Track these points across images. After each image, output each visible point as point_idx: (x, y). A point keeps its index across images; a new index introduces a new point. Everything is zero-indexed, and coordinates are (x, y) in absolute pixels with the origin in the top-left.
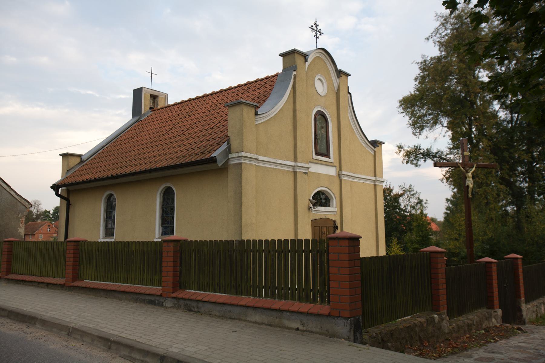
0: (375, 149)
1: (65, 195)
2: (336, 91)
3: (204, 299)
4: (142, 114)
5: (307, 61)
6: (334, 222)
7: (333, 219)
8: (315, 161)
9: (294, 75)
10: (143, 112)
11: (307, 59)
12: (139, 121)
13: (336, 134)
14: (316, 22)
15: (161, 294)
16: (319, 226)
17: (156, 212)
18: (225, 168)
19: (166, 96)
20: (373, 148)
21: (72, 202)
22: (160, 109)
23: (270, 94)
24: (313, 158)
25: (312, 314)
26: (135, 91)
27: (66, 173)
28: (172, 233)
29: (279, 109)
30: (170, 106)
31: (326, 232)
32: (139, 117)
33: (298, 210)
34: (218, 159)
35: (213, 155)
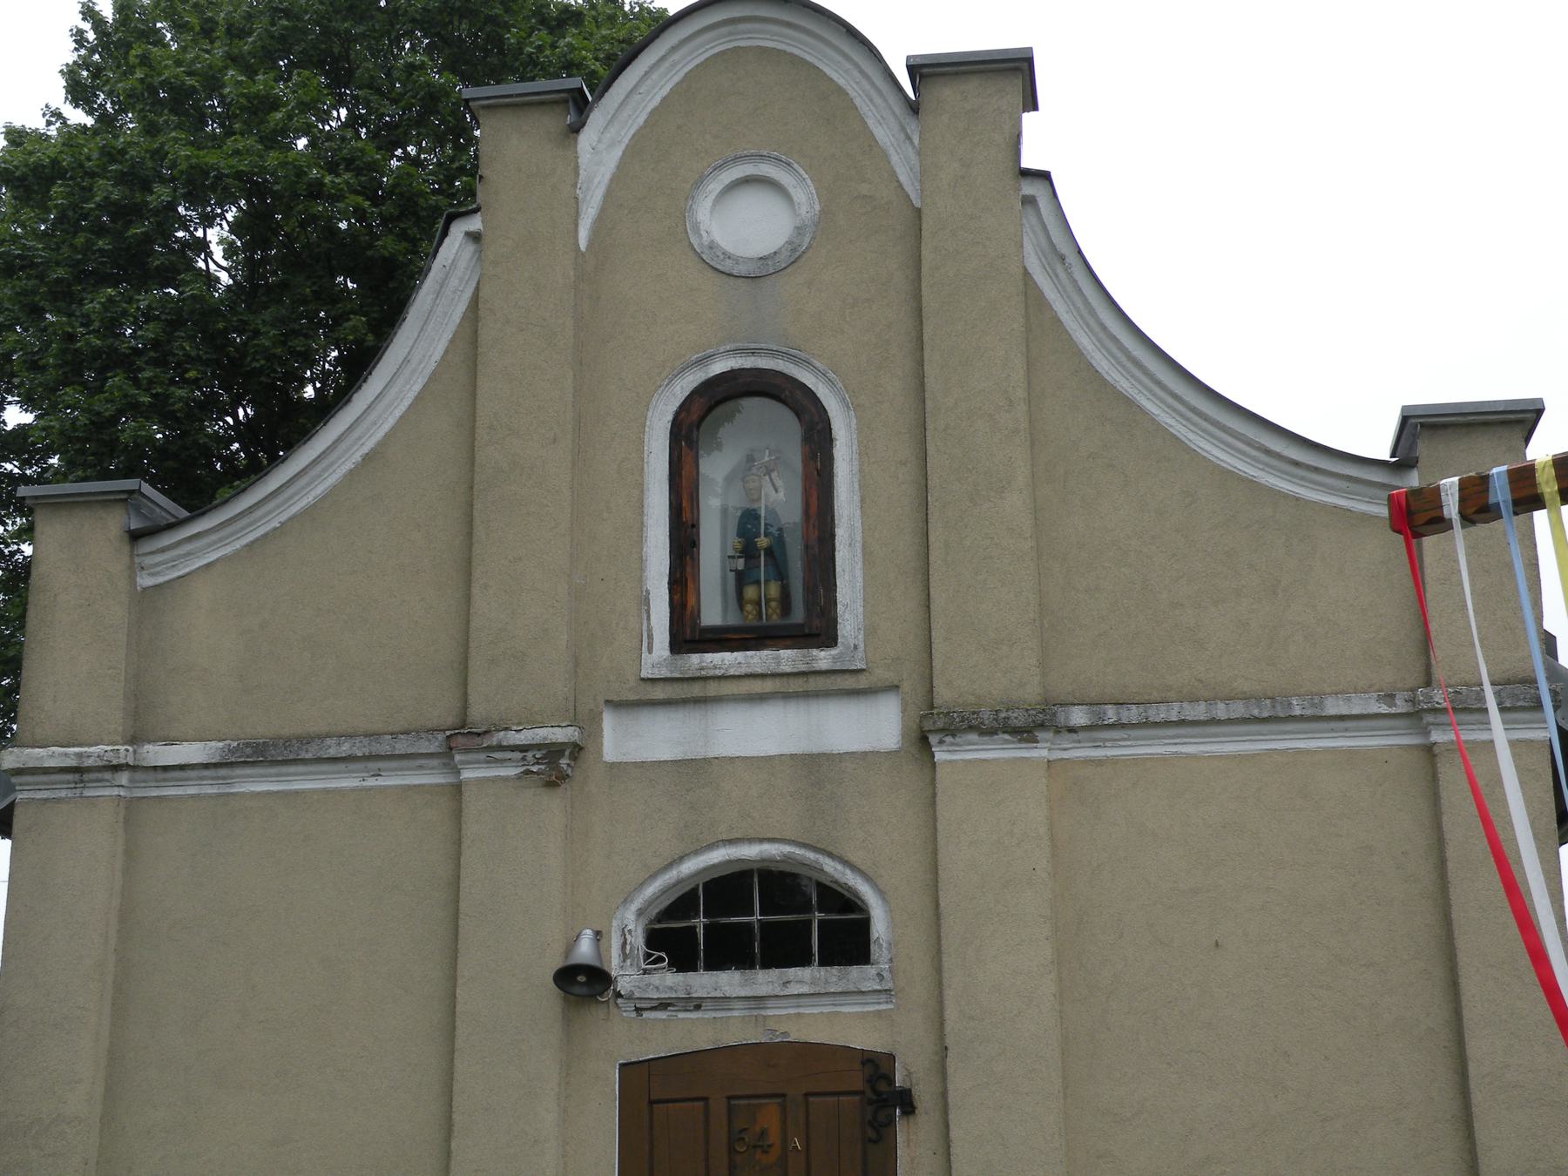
6: (877, 1067)
8: (659, 693)
24: (644, 674)
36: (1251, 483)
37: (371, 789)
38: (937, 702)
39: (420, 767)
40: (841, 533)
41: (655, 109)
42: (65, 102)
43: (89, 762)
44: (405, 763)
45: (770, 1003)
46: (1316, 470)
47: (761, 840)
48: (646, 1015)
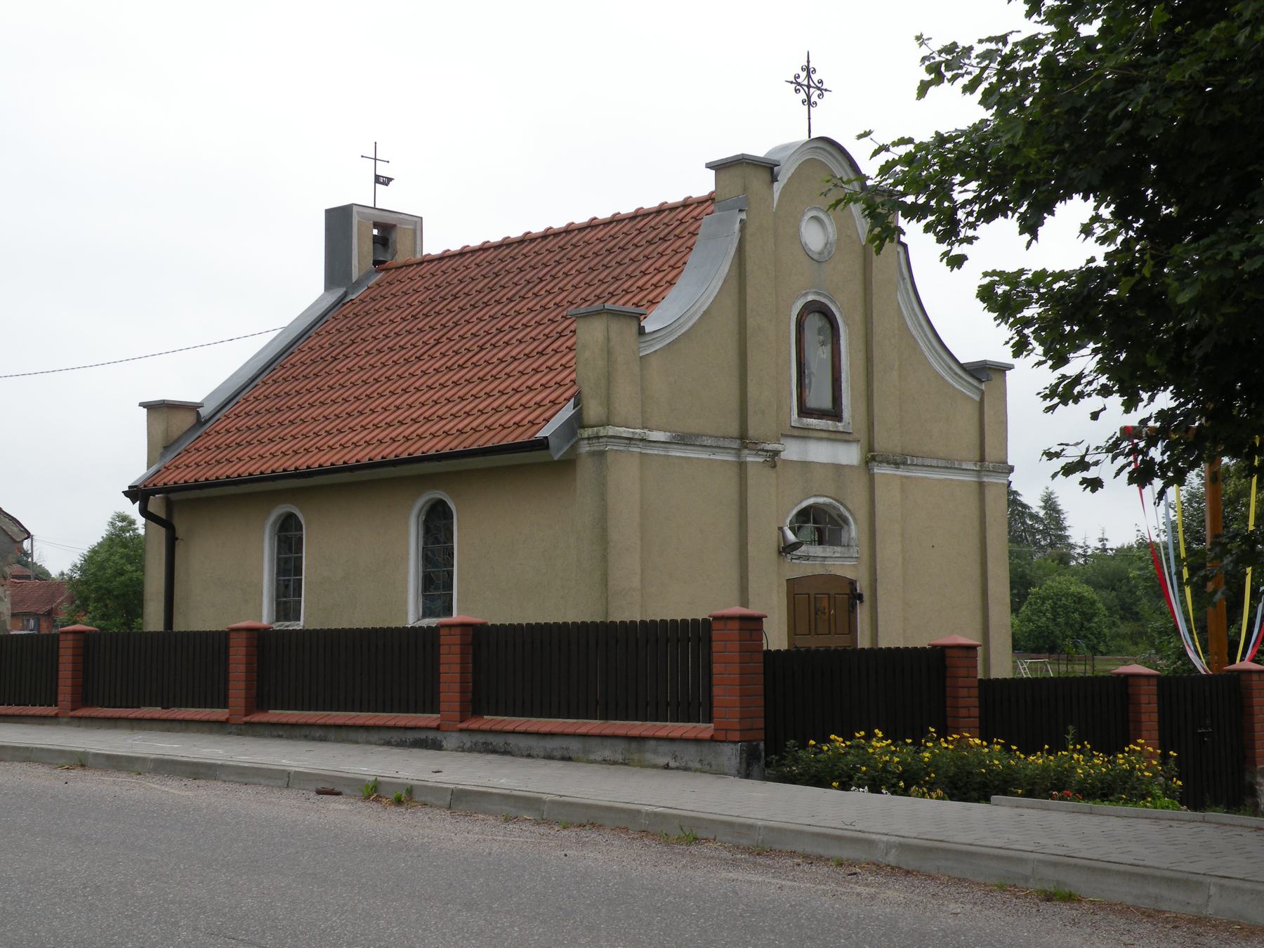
0: (983, 387)
1: (162, 514)
2: (864, 244)
3: (518, 729)
4: (354, 281)
5: (777, 181)
6: (852, 583)
7: (850, 575)
8: (796, 433)
9: (741, 221)
10: (355, 277)
11: (778, 174)
12: (346, 301)
13: (861, 356)
14: (808, 62)
15: (438, 725)
16: (809, 594)
17: (408, 559)
18: (568, 465)
19: (416, 224)
20: (975, 383)
21: (180, 531)
22: (402, 267)
23: (685, 263)
24: (793, 424)
25: (687, 740)
26: (330, 213)
27: (163, 455)
28: (448, 611)
29: (701, 312)
30: (431, 260)
31: (827, 610)
32: (345, 289)
33: (749, 555)
34: (552, 443)
35: (540, 435)
36: (942, 378)
37: (711, 460)
38: (877, 447)
39: (728, 453)
40: (843, 376)
41: (790, 178)
42: (941, 260)
43: (636, 437)
44: (724, 451)
45: (828, 559)
46: (961, 377)
47: (826, 496)
48: (794, 561)
